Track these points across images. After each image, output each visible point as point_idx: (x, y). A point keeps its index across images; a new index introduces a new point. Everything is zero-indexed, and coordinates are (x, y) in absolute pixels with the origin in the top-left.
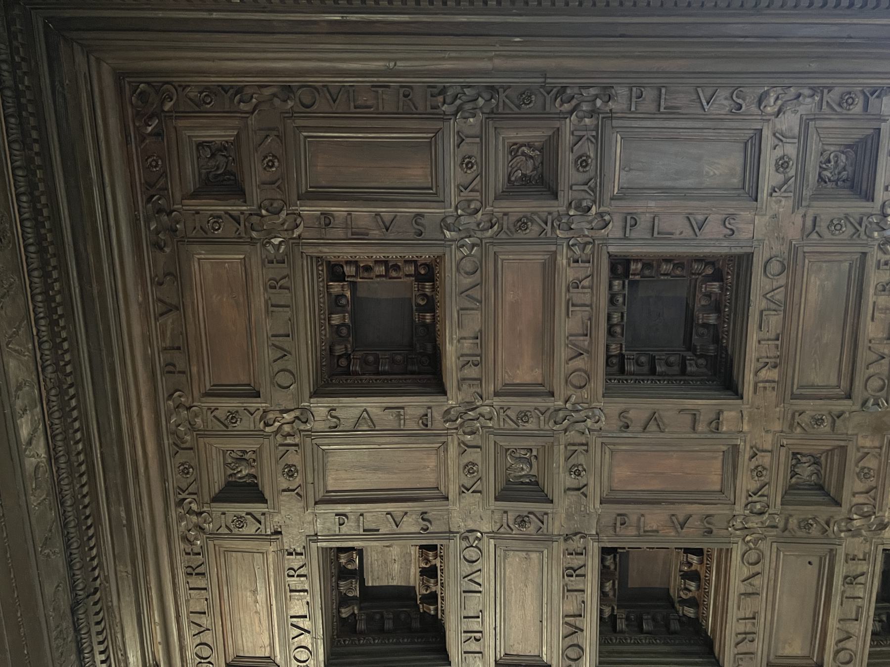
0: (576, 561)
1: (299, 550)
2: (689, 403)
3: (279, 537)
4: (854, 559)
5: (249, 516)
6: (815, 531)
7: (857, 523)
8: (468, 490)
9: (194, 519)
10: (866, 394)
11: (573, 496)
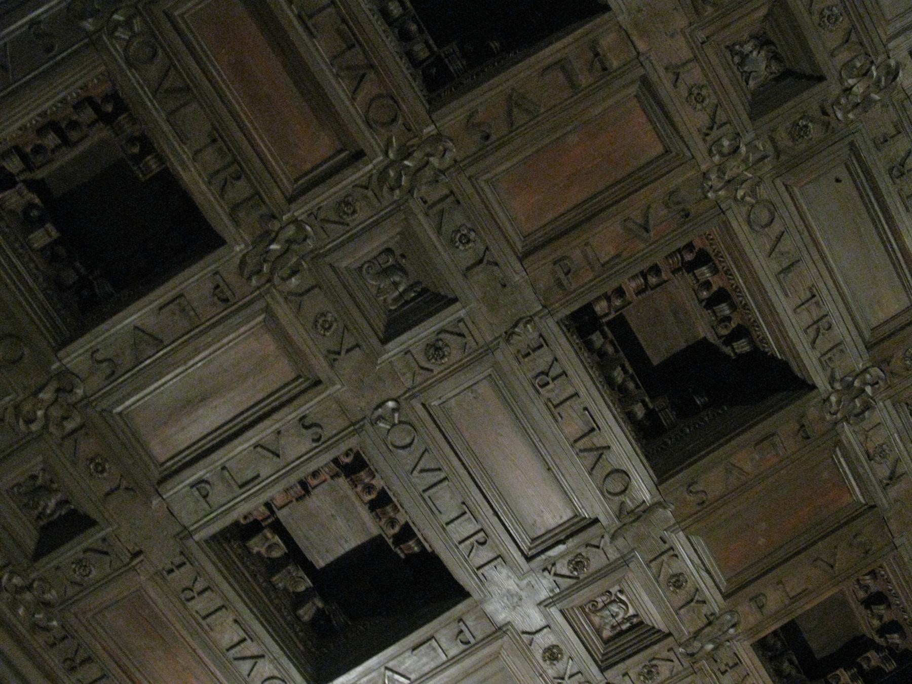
0: (543, 359)
1: (178, 560)
3: (142, 557)
4: (886, 141)
5: (88, 554)
6: (815, 131)
7: (859, 89)
8: (339, 353)
9: (28, 596)
11: (480, 275)
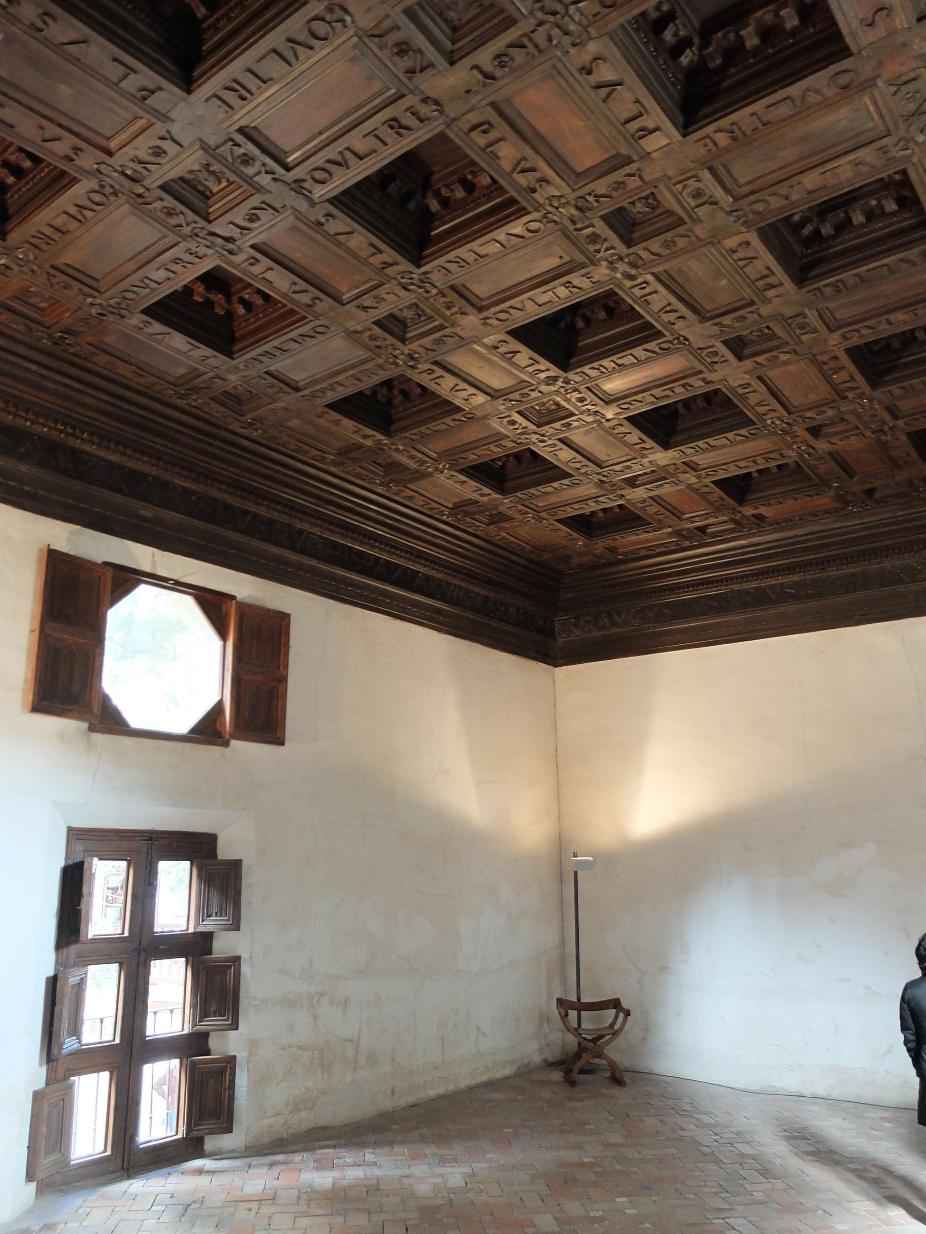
2: (650, 103)
10: (745, 207)
